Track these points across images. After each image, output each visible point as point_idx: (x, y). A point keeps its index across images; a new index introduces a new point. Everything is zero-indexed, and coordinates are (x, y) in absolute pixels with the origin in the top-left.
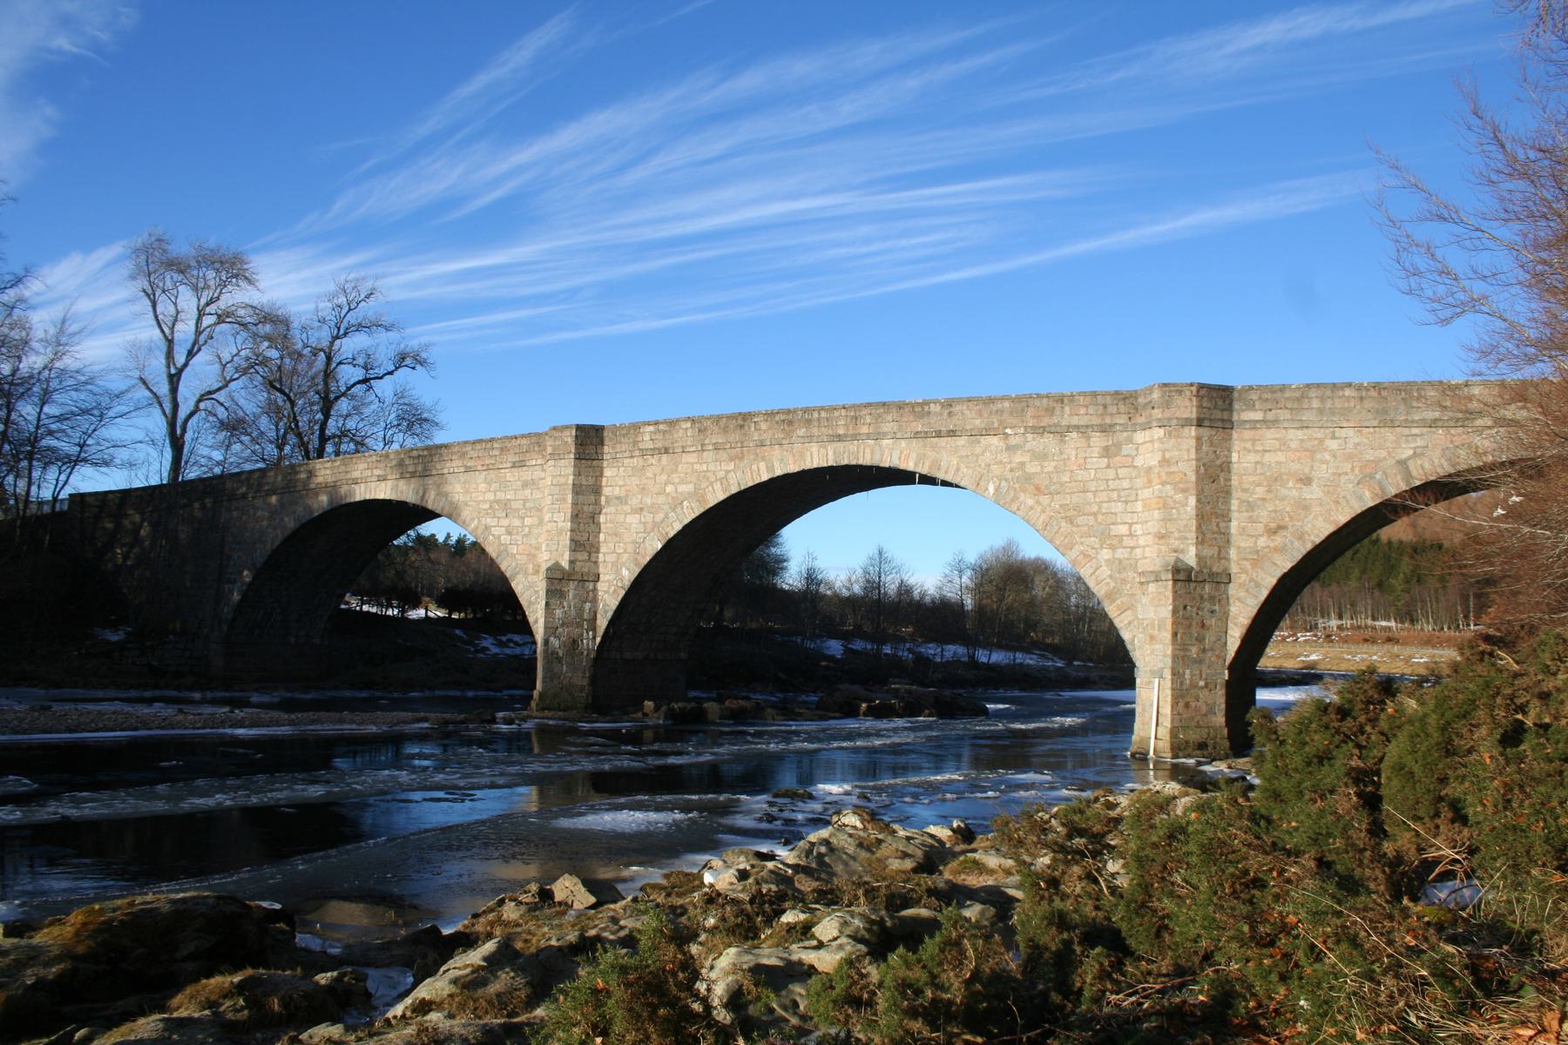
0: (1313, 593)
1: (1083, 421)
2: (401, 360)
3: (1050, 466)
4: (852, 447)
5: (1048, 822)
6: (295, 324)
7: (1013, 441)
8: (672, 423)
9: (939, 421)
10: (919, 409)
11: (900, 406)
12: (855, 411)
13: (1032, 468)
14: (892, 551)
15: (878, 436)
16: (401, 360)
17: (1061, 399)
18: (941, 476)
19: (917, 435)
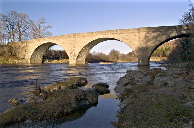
0: (42, 48)
1: (132, 32)
2: (49, 27)
3: (128, 37)
4: (105, 35)
5: (164, 90)
6: (143, 45)
7: (124, 34)
8: (84, 33)
9: (115, 33)
10: (113, 31)
11: (111, 31)
12: (106, 31)
13: (126, 37)
14: (95, 51)
15: (108, 34)
16: (49, 27)
17: (129, 29)
18: (118, 39)
19: (112, 34)
